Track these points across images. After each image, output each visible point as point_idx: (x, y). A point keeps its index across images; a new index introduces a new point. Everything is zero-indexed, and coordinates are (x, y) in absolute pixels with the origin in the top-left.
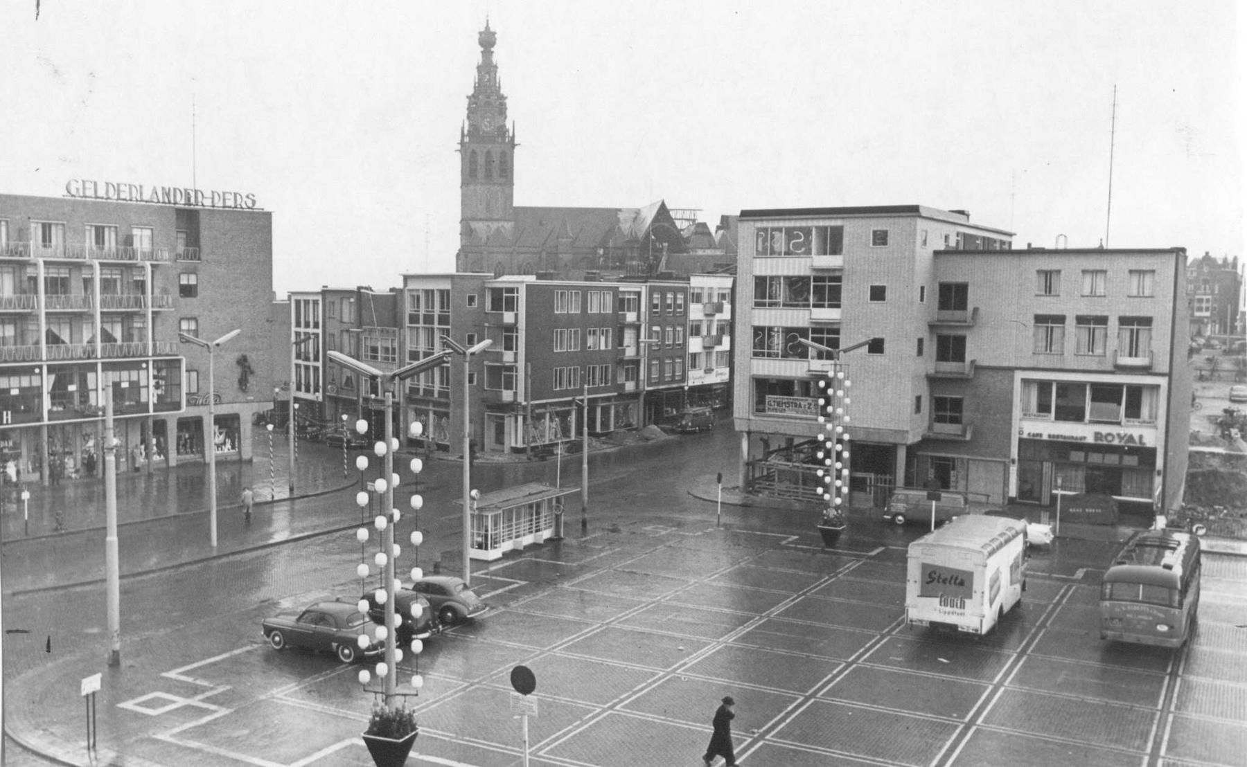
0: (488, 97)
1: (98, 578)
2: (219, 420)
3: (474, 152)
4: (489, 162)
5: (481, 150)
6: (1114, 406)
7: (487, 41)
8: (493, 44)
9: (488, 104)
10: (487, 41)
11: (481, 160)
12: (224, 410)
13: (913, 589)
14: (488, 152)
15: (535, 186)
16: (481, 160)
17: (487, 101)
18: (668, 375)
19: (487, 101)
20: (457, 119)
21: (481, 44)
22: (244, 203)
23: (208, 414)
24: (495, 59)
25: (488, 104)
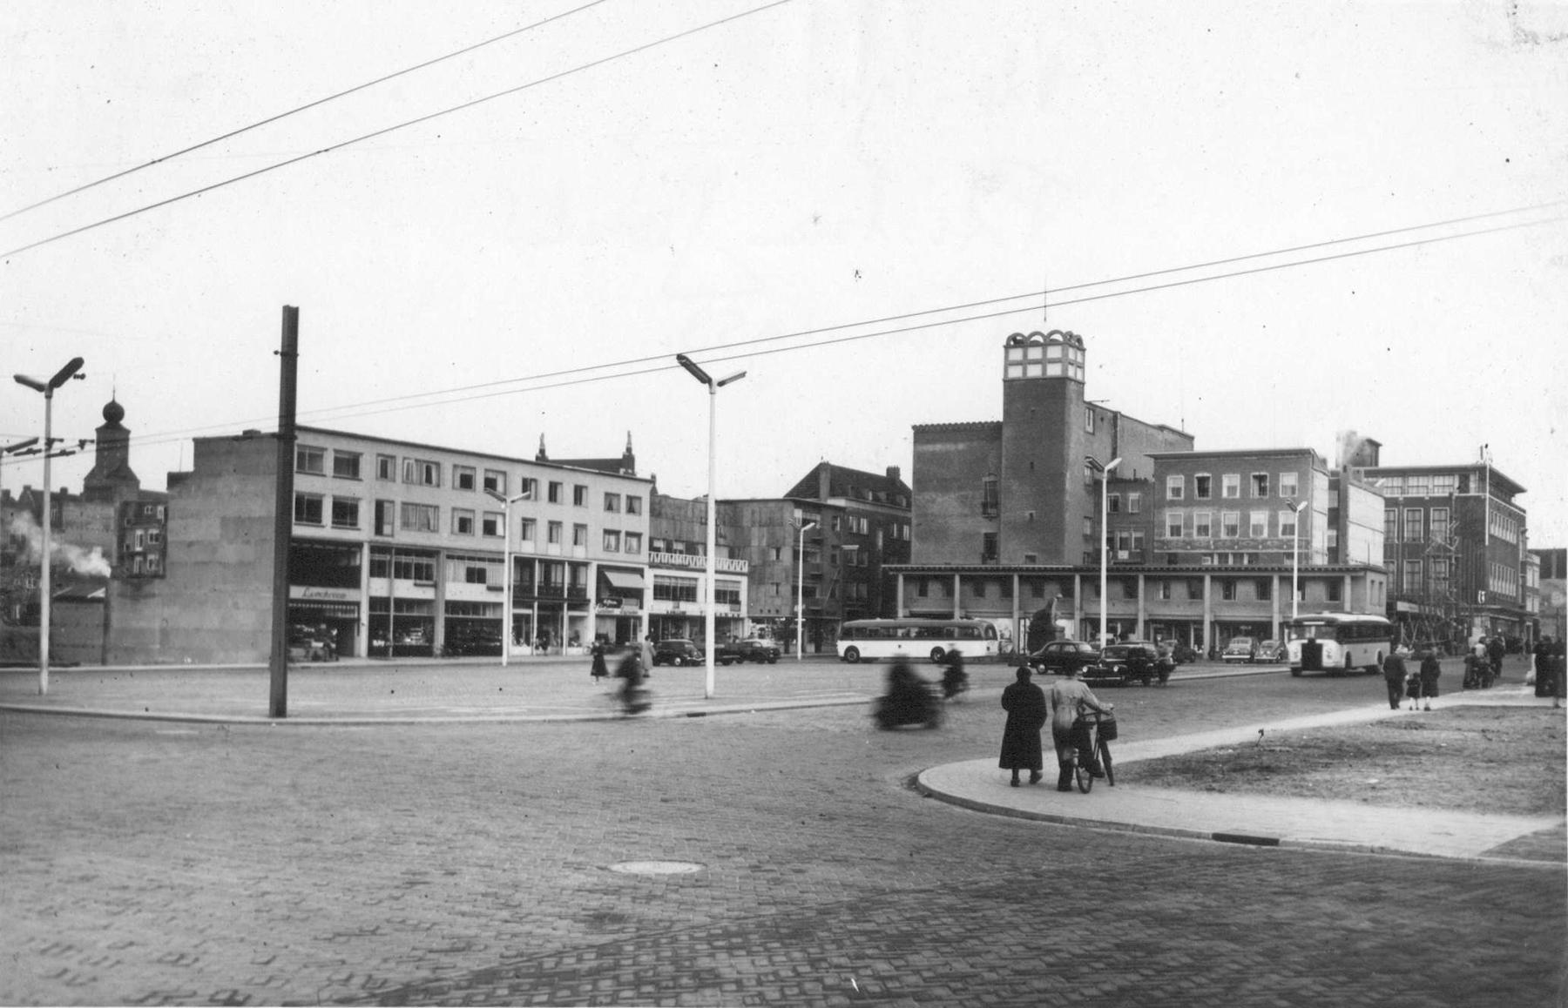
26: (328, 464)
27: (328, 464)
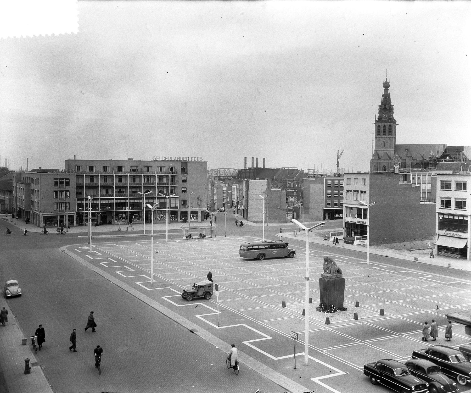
0: (385, 106)
1: (4, 160)
2: (192, 212)
3: (379, 126)
4: (384, 129)
5: (382, 125)
6: (320, 185)
7: (386, 86)
8: (389, 87)
9: (385, 108)
10: (386, 86)
11: (382, 129)
12: (194, 209)
13: (343, 232)
14: (385, 126)
15: (405, 135)
16: (382, 129)
17: (386, 107)
18: (150, 182)
19: (386, 107)
20: (376, 114)
21: (384, 87)
22: (200, 160)
23: (189, 211)
24: (389, 92)
25: (385, 108)
26: (453, 186)
27: (453, 186)
